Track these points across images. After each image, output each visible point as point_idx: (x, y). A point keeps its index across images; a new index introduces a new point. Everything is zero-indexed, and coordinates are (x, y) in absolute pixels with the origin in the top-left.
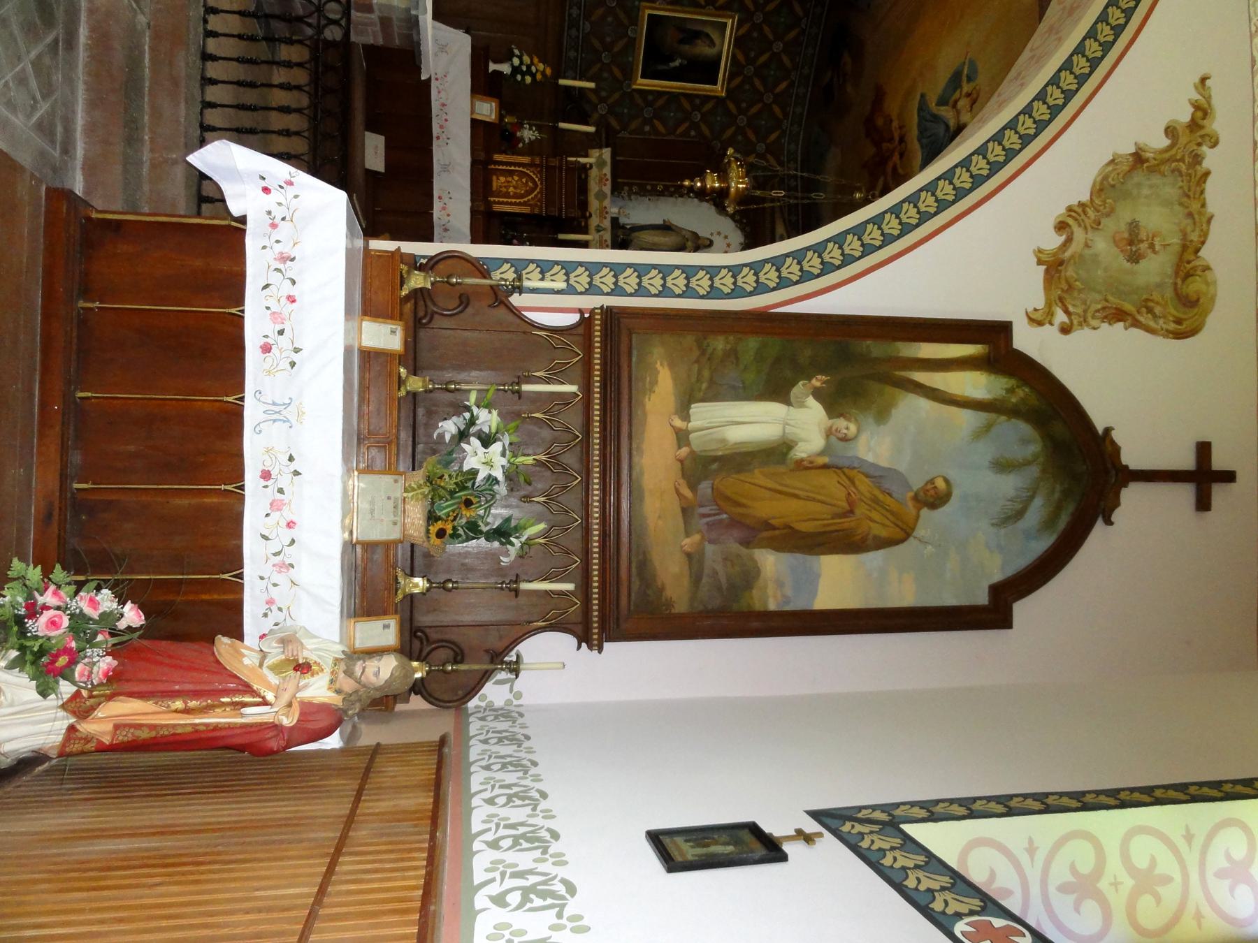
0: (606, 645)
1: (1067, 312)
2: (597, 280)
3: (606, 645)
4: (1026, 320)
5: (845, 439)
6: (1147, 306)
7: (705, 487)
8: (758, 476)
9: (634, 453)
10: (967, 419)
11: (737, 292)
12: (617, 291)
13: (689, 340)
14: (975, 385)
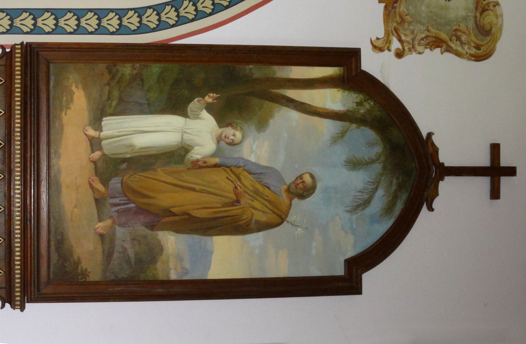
0: (27, 305)
1: (400, 40)
2: (17, 22)
3: (27, 305)
4: (371, 47)
5: (232, 144)
6: (456, 35)
7: (115, 183)
8: (161, 174)
9: (52, 155)
10: (328, 127)
11: (142, 29)
12: (35, 30)
13: (101, 67)
14: (333, 99)
